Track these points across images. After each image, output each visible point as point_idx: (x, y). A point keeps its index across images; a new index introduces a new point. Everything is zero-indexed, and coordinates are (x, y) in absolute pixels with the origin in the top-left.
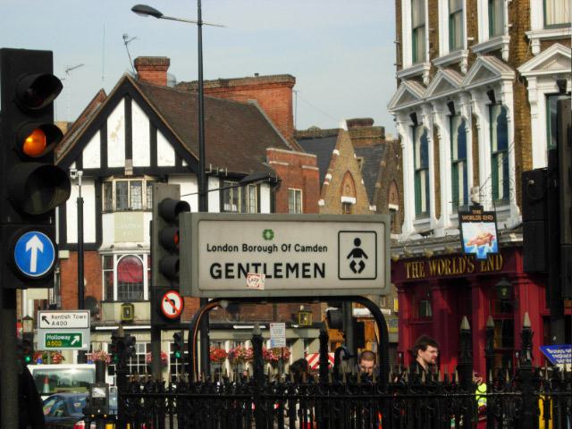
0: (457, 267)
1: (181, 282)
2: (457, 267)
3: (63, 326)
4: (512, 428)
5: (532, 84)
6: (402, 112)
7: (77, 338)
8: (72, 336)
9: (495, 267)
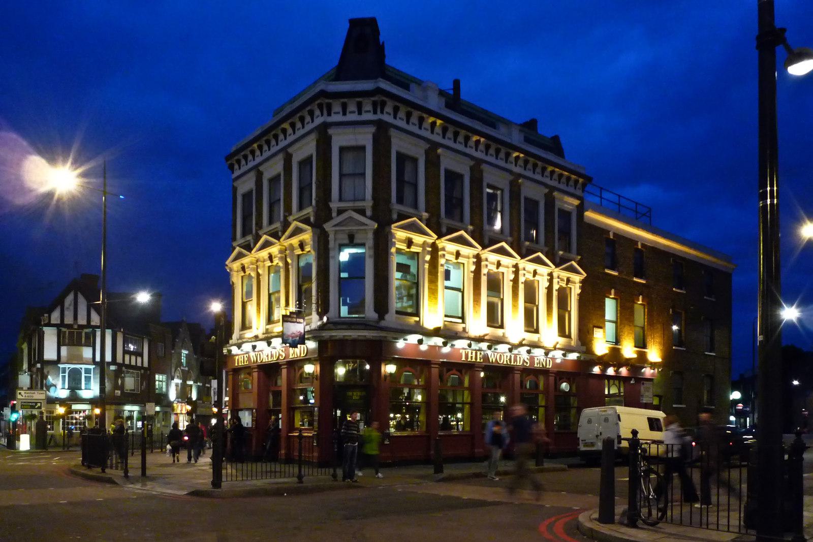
3: (31, 398)
4: (752, 536)
7: (39, 404)
8: (36, 403)
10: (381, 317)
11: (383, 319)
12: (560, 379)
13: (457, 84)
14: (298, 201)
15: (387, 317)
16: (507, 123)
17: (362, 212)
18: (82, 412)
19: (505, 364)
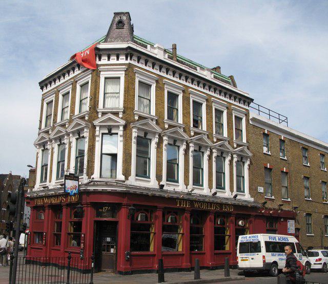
5: (98, 128)
6: (39, 145)
10: (127, 178)
11: (128, 179)
12: (238, 218)
13: (174, 48)
16: (202, 68)
17: (116, 114)
18: (12, 207)
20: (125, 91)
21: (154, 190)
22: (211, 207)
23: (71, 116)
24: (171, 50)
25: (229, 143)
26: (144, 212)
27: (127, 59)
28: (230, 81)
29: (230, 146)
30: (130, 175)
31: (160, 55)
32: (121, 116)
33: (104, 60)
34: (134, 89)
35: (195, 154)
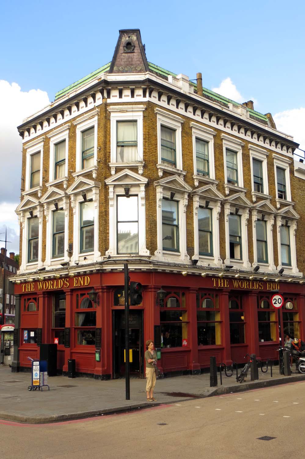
0: (57, 285)
1: (145, 247)
2: (57, 285)
5: (111, 189)
6: (24, 211)
9: (84, 283)
10: (152, 253)
13: (200, 79)
14: (173, 129)
15: (156, 253)
17: (134, 169)
19: (245, 289)
20: (144, 139)
21: (184, 266)
22: (253, 285)
23: (70, 173)
24: (195, 82)
25: (271, 203)
26: (175, 295)
27: (144, 96)
28: (267, 120)
29: (219, 192)
30: (156, 249)
31: (185, 89)
32: (141, 172)
33: (114, 97)
34: (156, 136)
35: (231, 217)
